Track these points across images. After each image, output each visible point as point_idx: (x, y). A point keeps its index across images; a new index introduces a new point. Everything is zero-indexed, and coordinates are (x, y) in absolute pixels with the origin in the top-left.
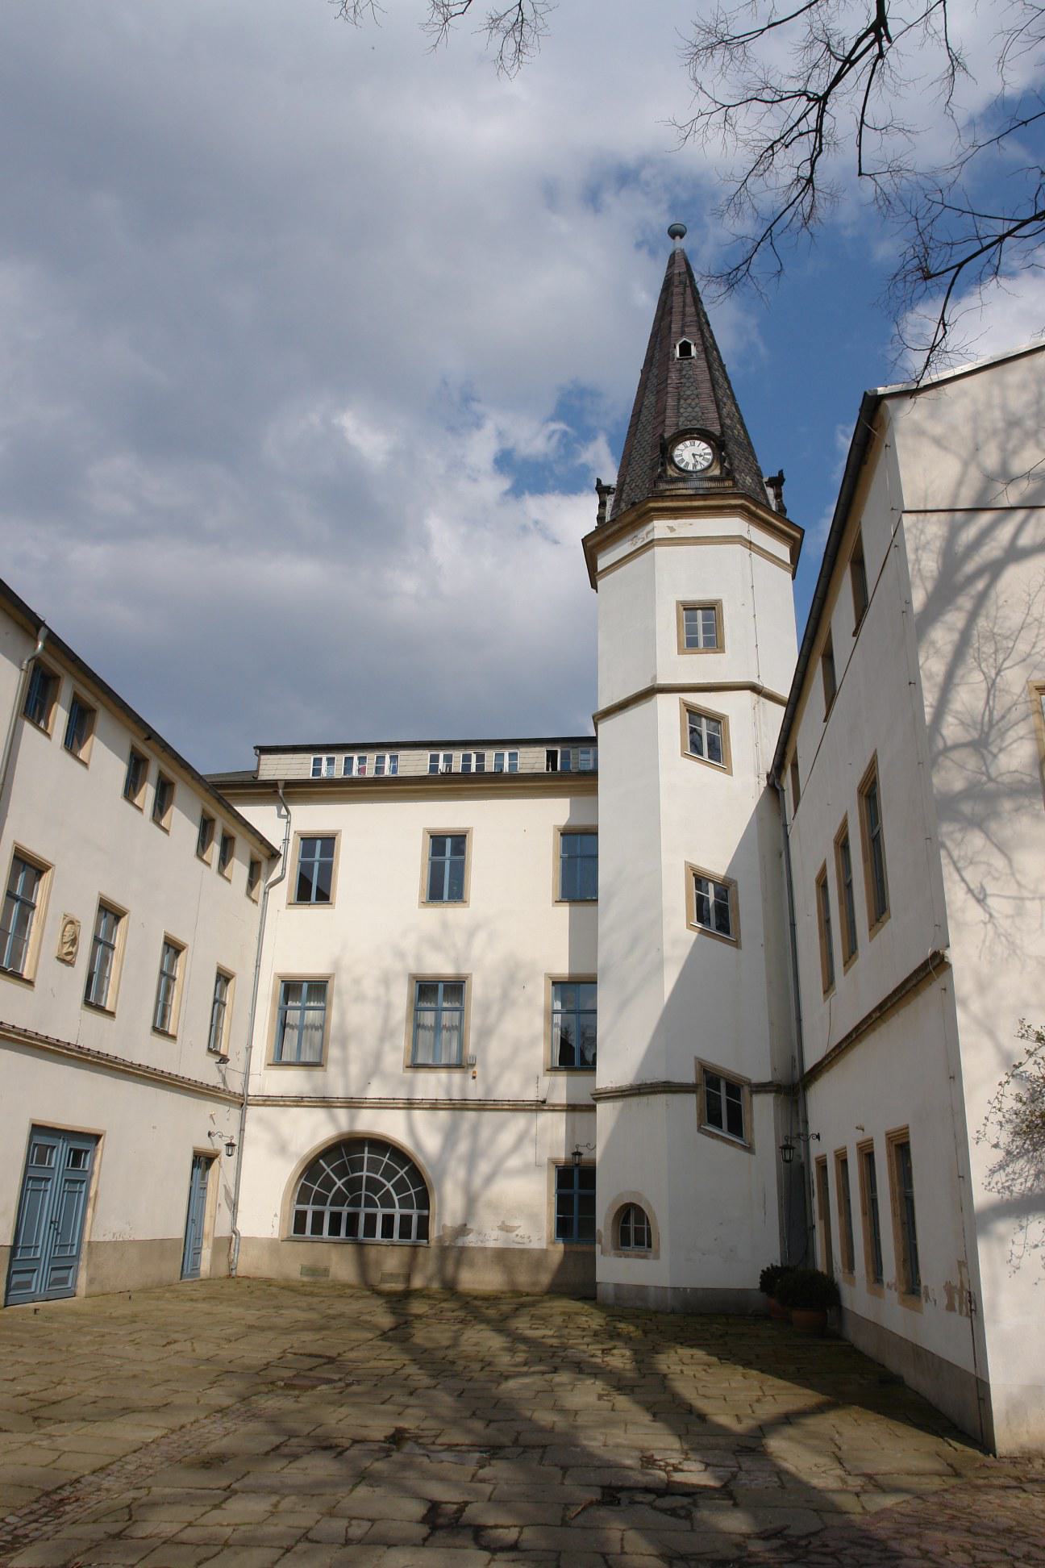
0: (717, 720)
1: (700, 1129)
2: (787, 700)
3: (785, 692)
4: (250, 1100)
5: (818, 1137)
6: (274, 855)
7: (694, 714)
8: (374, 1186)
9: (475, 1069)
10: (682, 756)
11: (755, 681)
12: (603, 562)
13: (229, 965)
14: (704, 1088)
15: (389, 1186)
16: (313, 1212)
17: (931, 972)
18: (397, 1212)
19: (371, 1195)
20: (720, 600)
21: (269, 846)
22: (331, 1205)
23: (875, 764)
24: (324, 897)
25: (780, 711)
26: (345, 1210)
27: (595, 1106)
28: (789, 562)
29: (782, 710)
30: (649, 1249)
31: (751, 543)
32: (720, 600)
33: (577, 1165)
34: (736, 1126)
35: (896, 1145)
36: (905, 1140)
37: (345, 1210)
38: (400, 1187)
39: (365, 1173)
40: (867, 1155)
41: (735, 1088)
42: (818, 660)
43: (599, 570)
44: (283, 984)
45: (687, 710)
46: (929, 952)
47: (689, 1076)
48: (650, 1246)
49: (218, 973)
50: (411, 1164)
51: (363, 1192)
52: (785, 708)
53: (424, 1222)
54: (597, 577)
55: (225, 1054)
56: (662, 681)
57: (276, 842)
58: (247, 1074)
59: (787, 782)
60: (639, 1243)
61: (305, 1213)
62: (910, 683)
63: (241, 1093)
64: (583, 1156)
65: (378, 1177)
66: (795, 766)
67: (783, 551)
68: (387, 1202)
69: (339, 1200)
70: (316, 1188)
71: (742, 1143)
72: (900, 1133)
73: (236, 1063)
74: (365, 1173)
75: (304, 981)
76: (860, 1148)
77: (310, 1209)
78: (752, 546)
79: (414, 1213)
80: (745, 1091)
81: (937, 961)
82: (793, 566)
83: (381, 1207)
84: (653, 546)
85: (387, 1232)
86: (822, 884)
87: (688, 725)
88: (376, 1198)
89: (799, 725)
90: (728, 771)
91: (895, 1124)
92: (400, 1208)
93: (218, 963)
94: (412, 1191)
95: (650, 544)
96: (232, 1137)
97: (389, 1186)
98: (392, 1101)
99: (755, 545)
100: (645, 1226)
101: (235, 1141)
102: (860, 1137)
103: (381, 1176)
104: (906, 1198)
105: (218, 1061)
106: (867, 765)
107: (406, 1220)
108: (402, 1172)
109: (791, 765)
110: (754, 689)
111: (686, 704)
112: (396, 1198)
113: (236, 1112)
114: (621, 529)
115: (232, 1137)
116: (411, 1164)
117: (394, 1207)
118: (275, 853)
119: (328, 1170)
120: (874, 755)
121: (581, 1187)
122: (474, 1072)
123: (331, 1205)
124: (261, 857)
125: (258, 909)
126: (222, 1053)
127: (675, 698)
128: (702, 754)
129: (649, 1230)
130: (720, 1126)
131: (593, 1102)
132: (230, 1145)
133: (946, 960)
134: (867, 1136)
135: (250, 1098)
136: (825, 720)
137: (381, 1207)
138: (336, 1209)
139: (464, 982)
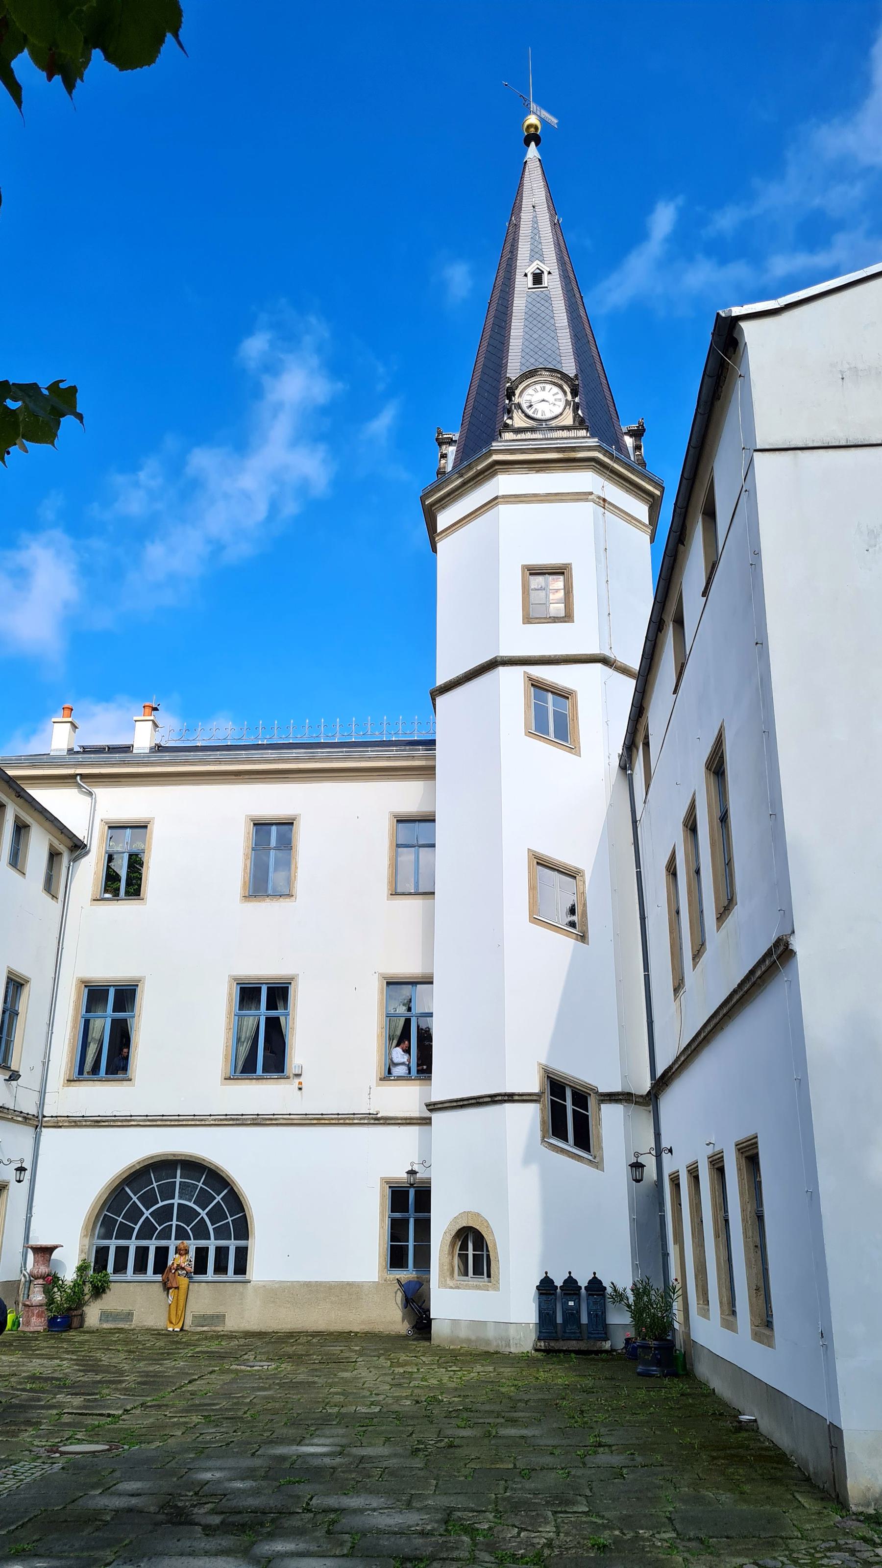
0: (564, 695)
1: (543, 1141)
2: (637, 672)
3: (635, 664)
4: (46, 1122)
5: (670, 1151)
6: (78, 848)
7: (538, 686)
8: (186, 1214)
9: (301, 1079)
10: (526, 735)
11: (607, 653)
12: (444, 520)
13: (23, 969)
14: (547, 1098)
15: (203, 1214)
16: (236, 1248)
17: (775, 961)
18: (212, 1244)
19: (182, 1225)
20: (570, 564)
21: (70, 836)
22: (137, 1238)
23: (723, 737)
24: (135, 889)
25: (631, 684)
26: (153, 1245)
27: (430, 1119)
28: (647, 522)
29: (633, 682)
30: (239, 1278)
31: (604, 500)
32: (570, 564)
33: (412, 1185)
34: (583, 1140)
35: (746, 1157)
36: (755, 1151)
37: (153, 1245)
38: (216, 1215)
39: (147, 1214)
40: (718, 1166)
41: (581, 1098)
42: (669, 626)
43: (438, 531)
44: (86, 990)
45: (532, 685)
46: (774, 939)
47: (533, 1084)
48: (489, 1276)
49: (8, 978)
50: (229, 1188)
51: (174, 1222)
52: (635, 681)
53: (242, 1254)
54: (436, 539)
55: (16, 1069)
56: (506, 651)
57: (80, 833)
58: (43, 1093)
59: (640, 764)
60: (478, 1271)
61: (147, 1249)
62: (757, 643)
63: (36, 1114)
64: (418, 1175)
65: (191, 1204)
66: (646, 745)
67: (641, 511)
68: (201, 1232)
69: (147, 1232)
70: (120, 1219)
71: (590, 1158)
72: (750, 1142)
73: (29, 1079)
74: (176, 1201)
75: (110, 986)
76: (711, 1162)
77: (113, 1244)
78: (606, 505)
79: (232, 1245)
80: (592, 1102)
81: (782, 948)
82: (652, 527)
83: (194, 1239)
84: (497, 504)
85: (140, 1267)
86: (672, 871)
87: (533, 701)
88: (188, 1229)
89: (651, 698)
90: (574, 749)
91: (743, 1135)
92: (215, 1240)
93: (8, 967)
94: (230, 1219)
95: (494, 502)
96: (22, 1161)
97: (203, 1214)
98: (177, 1117)
99: (610, 503)
100: (485, 1253)
101: (27, 1165)
102: (710, 1151)
103: (194, 1203)
104: (758, 1217)
105: (7, 1078)
106: (715, 736)
107: (222, 1253)
108: (219, 1198)
109: (643, 744)
110: (605, 661)
111: (530, 679)
112: (211, 1228)
113: (29, 1131)
114: (464, 484)
115: (22, 1161)
116: (229, 1188)
117: (209, 1239)
118: (79, 843)
119: (135, 1198)
120: (720, 730)
121: (417, 1210)
122: (300, 1083)
123: (137, 1238)
124: (62, 848)
125: (57, 906)
126: (12, 1068)
127: (519, 671)
128: (548, 734)
129: (488, 1256)
130: (565, 1139)
131: (427, 1114)
132: (21, 1169)
133: (790, 947)
134: (717, 1149)
135: (45, 1119)
136: (675, 692)
137: (194, 1239)
138: (144, 1243)
139: (290, 983)
